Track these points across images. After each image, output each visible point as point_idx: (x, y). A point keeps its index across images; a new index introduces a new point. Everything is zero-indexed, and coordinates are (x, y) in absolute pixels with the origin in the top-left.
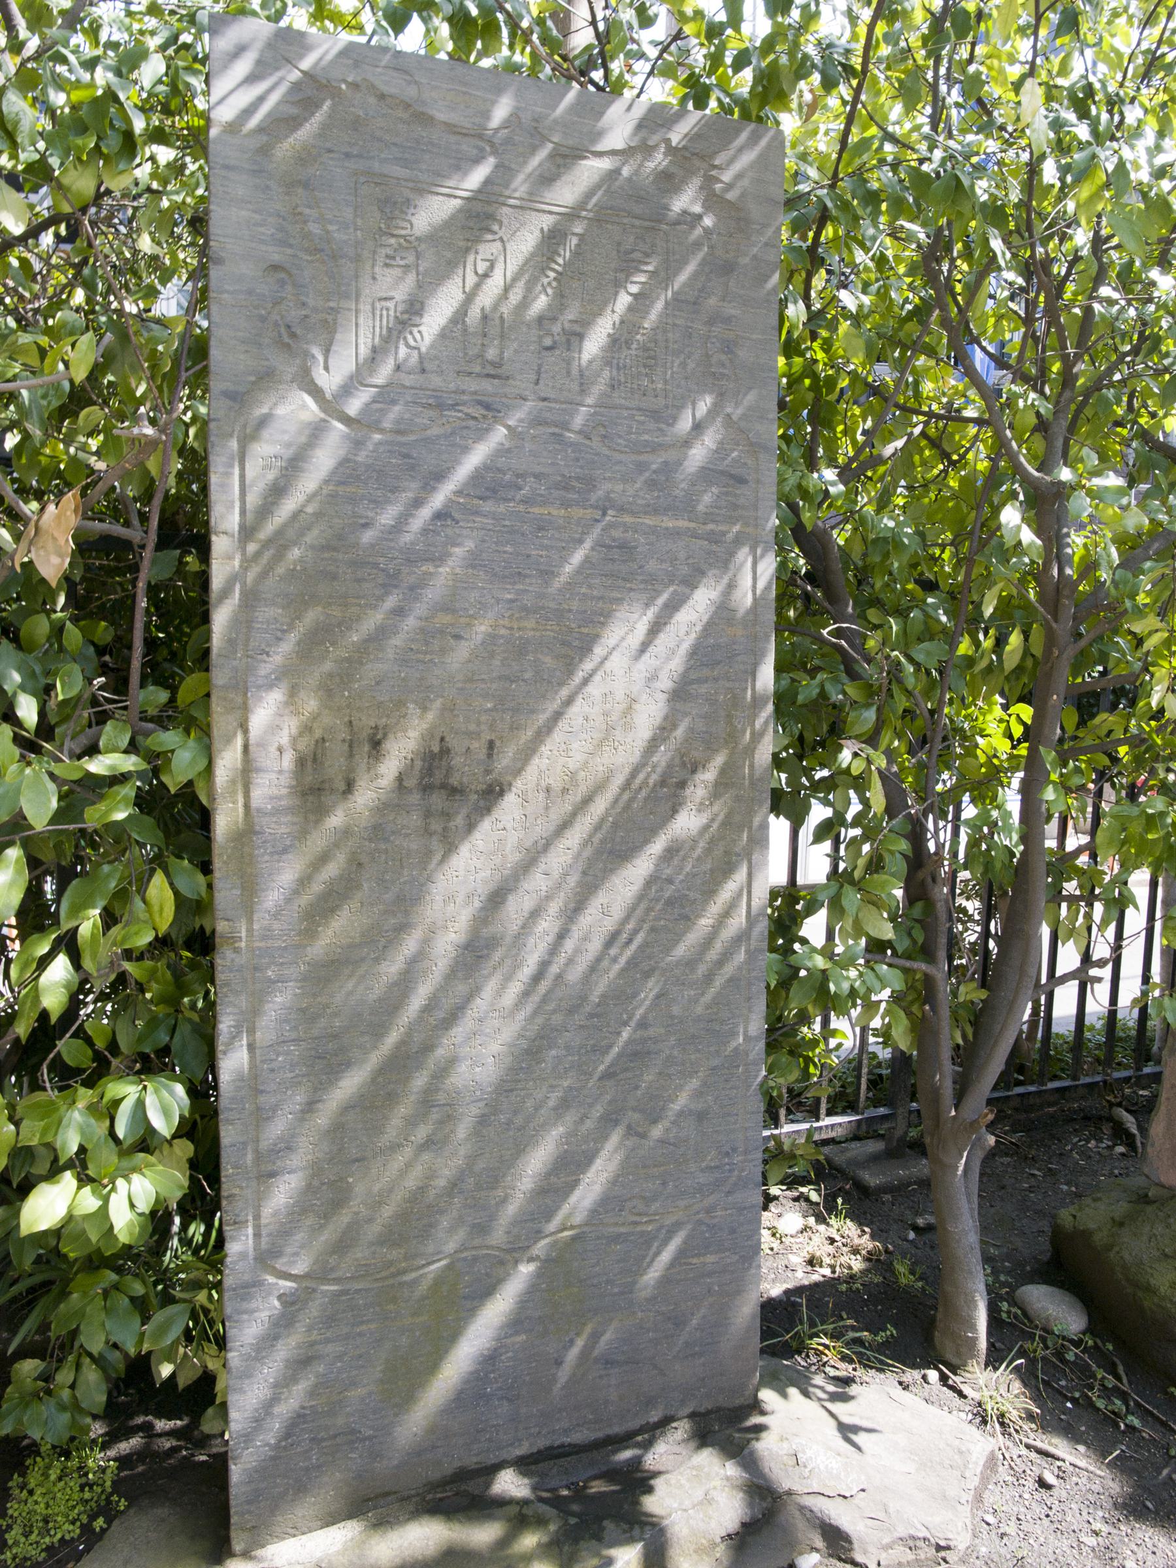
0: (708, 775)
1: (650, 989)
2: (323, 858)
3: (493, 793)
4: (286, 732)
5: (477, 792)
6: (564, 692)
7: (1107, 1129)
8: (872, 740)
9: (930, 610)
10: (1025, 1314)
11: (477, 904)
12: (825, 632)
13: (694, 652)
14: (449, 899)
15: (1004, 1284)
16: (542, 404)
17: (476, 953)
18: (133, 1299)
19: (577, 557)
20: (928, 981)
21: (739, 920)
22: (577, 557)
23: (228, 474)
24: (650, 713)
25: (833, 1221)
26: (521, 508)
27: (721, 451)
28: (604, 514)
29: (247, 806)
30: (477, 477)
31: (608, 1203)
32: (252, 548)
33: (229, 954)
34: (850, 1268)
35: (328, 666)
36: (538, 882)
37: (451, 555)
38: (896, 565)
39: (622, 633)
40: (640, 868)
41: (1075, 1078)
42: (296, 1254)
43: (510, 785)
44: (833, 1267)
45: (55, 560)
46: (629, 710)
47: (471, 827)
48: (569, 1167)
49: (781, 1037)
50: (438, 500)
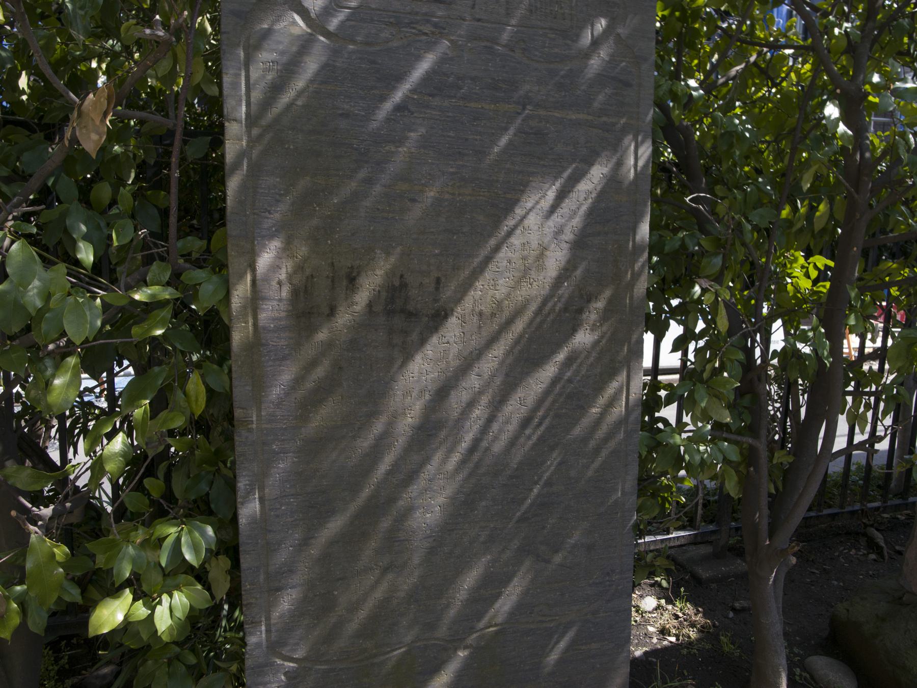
0: (600, 304)
1: (554, 459)
2: (313, 364)
3: (439, 317)
4: (284, 270)
5: (427, 316)
6: (493, 242)
7: (863, 541)
8: (718, 279)
9: (760, 185)
10: (812, 677)
11: (427, 397)
12: (687, 199)
13: (591, 213)
14: (407, 393)
15: (796, 655)
16: (476, 23)
17: (429, 431)
18: (189, 667)
19: (504, 141)
20: (752, 450)
21: (620, 409)
22: (504, 141)
23: (238, 75)
24: (556, 259)
25: (677, 603)
26: (461, 103)
27: (612, 61)
28: (524, 109)
29: (255, 325)
30: (428, 78)
31: (520, 609)
32: (255, 131)
33: (244, 433)
34: (689, 637)
35: (315, 222)
36: (473, 381)
37: (407, 138)
38: (738, 153)
39: (537, 198)
40: (549, 371)
41: (842, 507)
42: (298, 644)
43: (452, 310)
44: (677, 636)
45: (94, 137)
46: (541, 256)
47: (423, 341)
48: (492, 585)
49: (647, 485)
50: (398, 96)
